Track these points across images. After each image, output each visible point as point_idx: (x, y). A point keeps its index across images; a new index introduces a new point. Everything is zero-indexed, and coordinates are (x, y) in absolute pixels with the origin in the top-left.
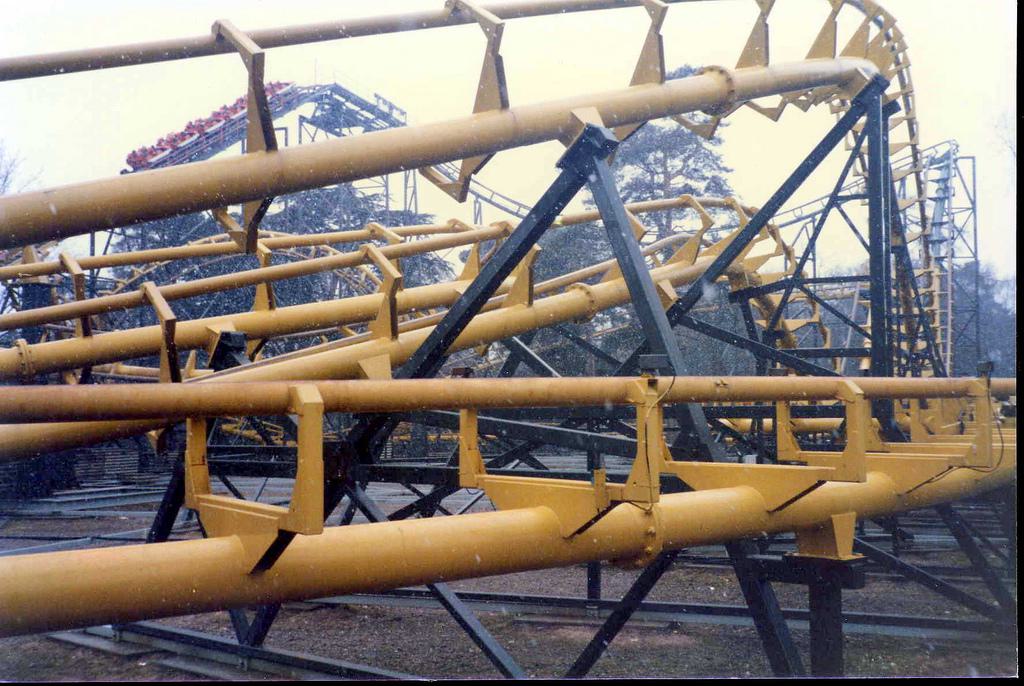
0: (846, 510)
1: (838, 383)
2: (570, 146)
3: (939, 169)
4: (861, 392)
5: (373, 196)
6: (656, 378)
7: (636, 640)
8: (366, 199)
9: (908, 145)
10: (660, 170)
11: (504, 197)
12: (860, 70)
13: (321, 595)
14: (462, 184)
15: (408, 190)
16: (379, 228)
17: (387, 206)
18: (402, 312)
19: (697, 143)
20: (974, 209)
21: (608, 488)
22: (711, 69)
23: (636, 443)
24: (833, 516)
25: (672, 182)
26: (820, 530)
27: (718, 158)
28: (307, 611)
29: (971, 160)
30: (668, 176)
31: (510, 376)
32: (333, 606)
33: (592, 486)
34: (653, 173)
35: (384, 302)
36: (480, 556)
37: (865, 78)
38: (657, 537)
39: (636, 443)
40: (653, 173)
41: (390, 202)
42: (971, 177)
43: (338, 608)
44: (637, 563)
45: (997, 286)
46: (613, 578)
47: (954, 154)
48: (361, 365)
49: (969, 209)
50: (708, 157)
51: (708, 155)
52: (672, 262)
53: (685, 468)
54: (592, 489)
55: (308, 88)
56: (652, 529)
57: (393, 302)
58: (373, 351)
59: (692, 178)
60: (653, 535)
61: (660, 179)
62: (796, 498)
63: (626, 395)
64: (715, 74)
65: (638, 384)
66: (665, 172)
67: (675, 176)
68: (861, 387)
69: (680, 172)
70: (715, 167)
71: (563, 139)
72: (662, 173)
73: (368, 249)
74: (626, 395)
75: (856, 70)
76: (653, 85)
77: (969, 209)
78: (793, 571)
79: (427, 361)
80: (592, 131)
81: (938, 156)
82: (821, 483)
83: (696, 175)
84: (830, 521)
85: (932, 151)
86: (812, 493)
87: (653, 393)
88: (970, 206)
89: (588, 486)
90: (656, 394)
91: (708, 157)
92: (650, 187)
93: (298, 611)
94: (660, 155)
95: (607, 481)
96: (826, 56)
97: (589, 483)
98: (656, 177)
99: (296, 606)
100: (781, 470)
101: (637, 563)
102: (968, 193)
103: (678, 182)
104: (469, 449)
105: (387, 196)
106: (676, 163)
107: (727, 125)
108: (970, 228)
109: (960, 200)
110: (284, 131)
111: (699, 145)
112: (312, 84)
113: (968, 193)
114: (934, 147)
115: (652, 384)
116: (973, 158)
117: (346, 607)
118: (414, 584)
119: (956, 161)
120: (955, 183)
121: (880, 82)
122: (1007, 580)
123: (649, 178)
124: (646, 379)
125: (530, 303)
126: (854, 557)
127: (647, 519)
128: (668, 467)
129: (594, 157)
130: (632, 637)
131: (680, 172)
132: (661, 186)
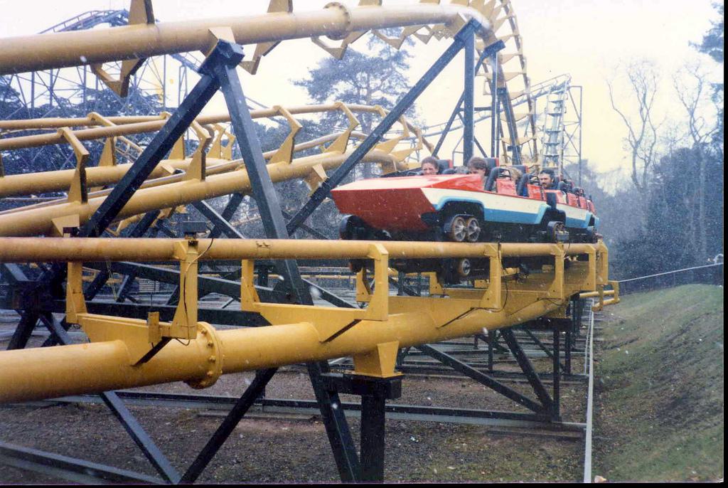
0: (390, 340)
1: (370, 245)
2: (209, 54)
3: (557, 93)
4: (386, 252)
5: (154, 96)
6: (197, 240)
7: (286, 429)
8: (149, 98)
9: (519, 73)
10: (364, 86)
11: (257, 103)
12: (460, 14)
13: (54, 396)
14: (122, 82)
15: (181, 93)
16: (98, 117)
17: (164, 104)
18: (93, 185)
19: (392, 67)
20: (580, 122)
21: (160, 326)
22: (334, 5)
23: (240, 286)
24: (379, 345)
25: (373, 95)
26: (369, 354)
27: (406, 80)
28: (42, 408)
29: (579, 89)
30: (370, 91)
31: (155, 237)
32: (65, 404)
33: (147, 324)
34: (359, 88)
35: (75, 174)
36: (487, 328)
37: (464, 21)
38: (217, 363)
39: (240, 286)
40: (359, 88)
41: (167, 101)
42: (163, 71)
43: (69, 405)
44: (201, 383)
45: (599, 177)
46: (290, 381)
47: (568, 83)
48: (54, 222)
49: (576, 123)
50: (399, 78)
51: (399, 78)
52: (330, 150)
53: (265, 308)
54: (147, 327)
55: (105, 12)
56: (213, 357)
57: (83, 175)
58: (66, 211)
59: (387, 93)
60: (214, 361)
61: (364, 92)
62: (453, 320)
63: (173, 253)
64: (336, 9)
65: (182, 245)
66: (368, 88)
67: (374, 90)
68: (387, 249)
69: (378, 88)
70: (404, 86)
71: (204, 52)
72: (366, 88)
73: (64, 132)
74: (173, 253)
75: (458, 14)
76: (283, 13)
77: (576, 123)
78: (356, 385)
79: (98, 224)
80: (224, 45)
81: (558, 85)
82: (357, 321)
83: (390, 91)
84: (376, 348)
85: (554, 81)
86: (346, 333)
87: (193, 251)
88: (578, 120)
89: (143, 324)
90: (195, 252)
91: (399, 78)
92: (357, 98)
93: (35, 408)
94: (365, 75)
95: (160, 321)
96: (461, 4)
97: (145, 321)
98: (361, 91)
99: (32, 404)
100: (345, 311)
101: (201, 383)
102: (577, 113)
103: (377, 95)
104: (74, 293)
105: (164, 96)
106: (375, 83)
107: (413, 57)
108: (577, 135)
109: (569, 116)
110: (579, 89)
111: (393, 69)
112: (107, 9)
113: (577, 113)
114: (555, 78)
115: (193, 244)
116: (581, 87)
117: (77, 405)
118: (133, 386)
119: (568, 88)
120: (567, 104)
121: (474, 24)
122: (564, 382)
123: (356, 91)
124: (187, 240)
125: (203, 178)
126: (395, 375)
127: (210, 350)
128: (255, 307)
129: (226, 66)
130: (284, 427)
131: (378, 88)
132: (364, 98)
